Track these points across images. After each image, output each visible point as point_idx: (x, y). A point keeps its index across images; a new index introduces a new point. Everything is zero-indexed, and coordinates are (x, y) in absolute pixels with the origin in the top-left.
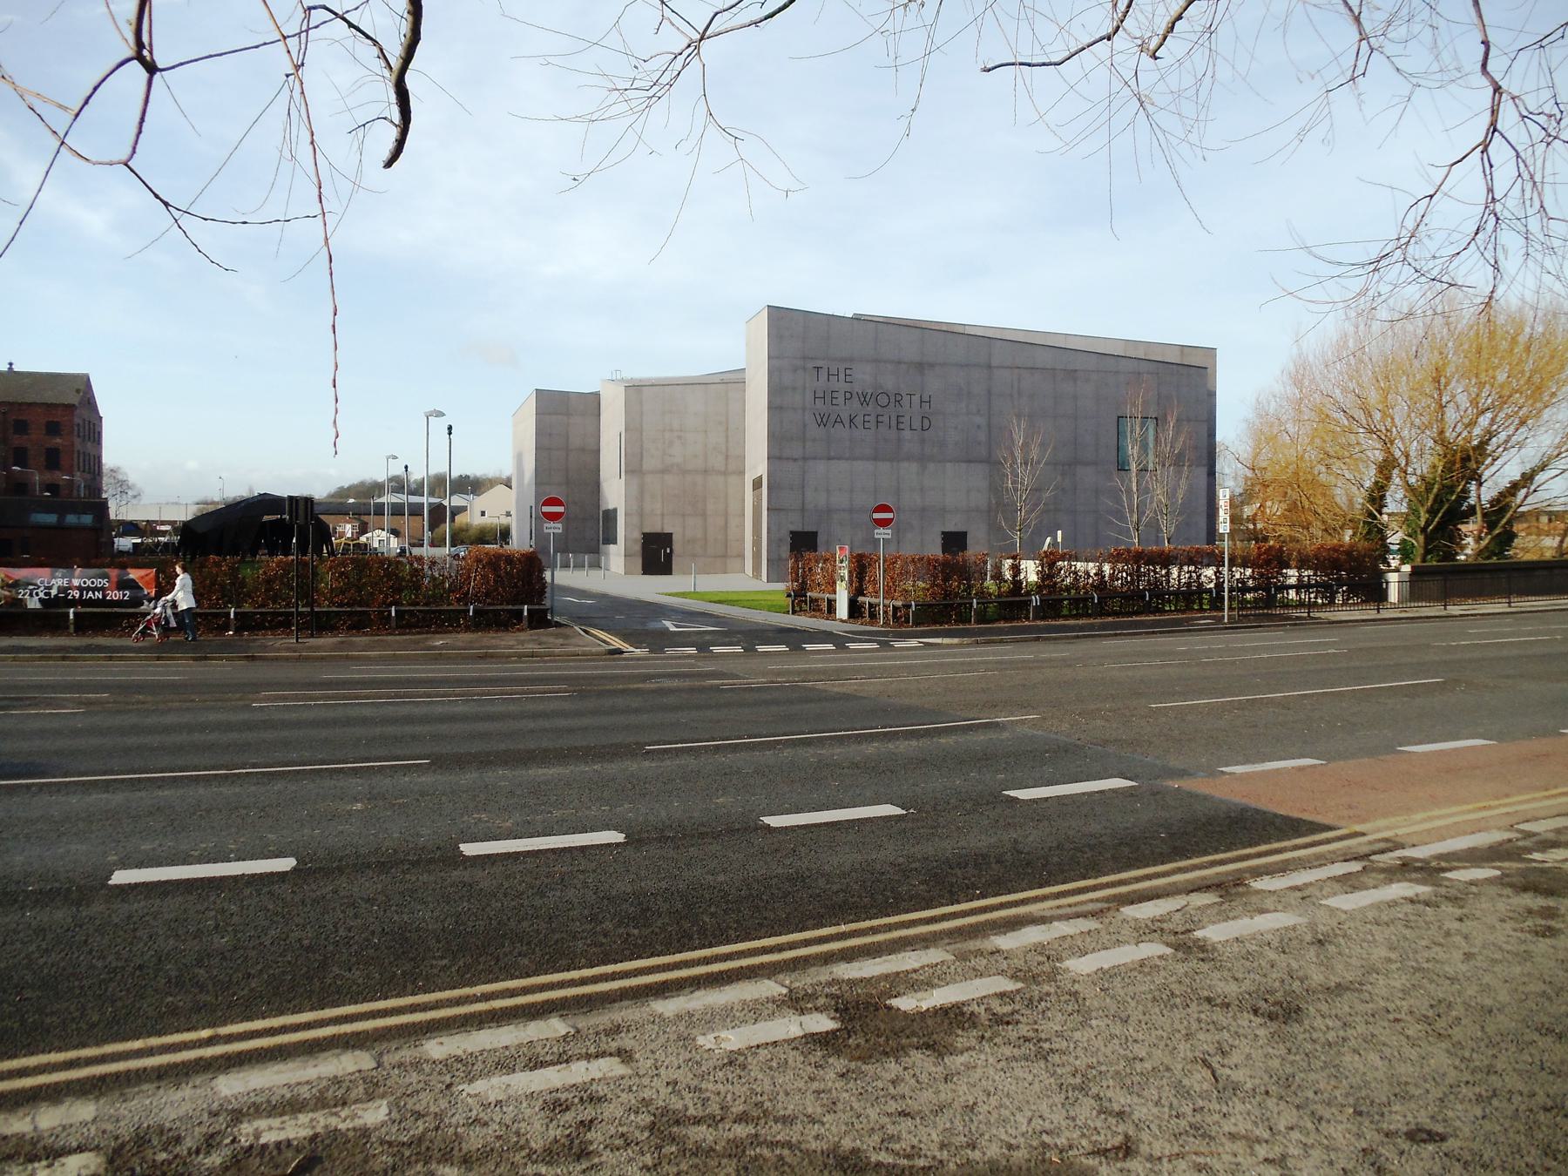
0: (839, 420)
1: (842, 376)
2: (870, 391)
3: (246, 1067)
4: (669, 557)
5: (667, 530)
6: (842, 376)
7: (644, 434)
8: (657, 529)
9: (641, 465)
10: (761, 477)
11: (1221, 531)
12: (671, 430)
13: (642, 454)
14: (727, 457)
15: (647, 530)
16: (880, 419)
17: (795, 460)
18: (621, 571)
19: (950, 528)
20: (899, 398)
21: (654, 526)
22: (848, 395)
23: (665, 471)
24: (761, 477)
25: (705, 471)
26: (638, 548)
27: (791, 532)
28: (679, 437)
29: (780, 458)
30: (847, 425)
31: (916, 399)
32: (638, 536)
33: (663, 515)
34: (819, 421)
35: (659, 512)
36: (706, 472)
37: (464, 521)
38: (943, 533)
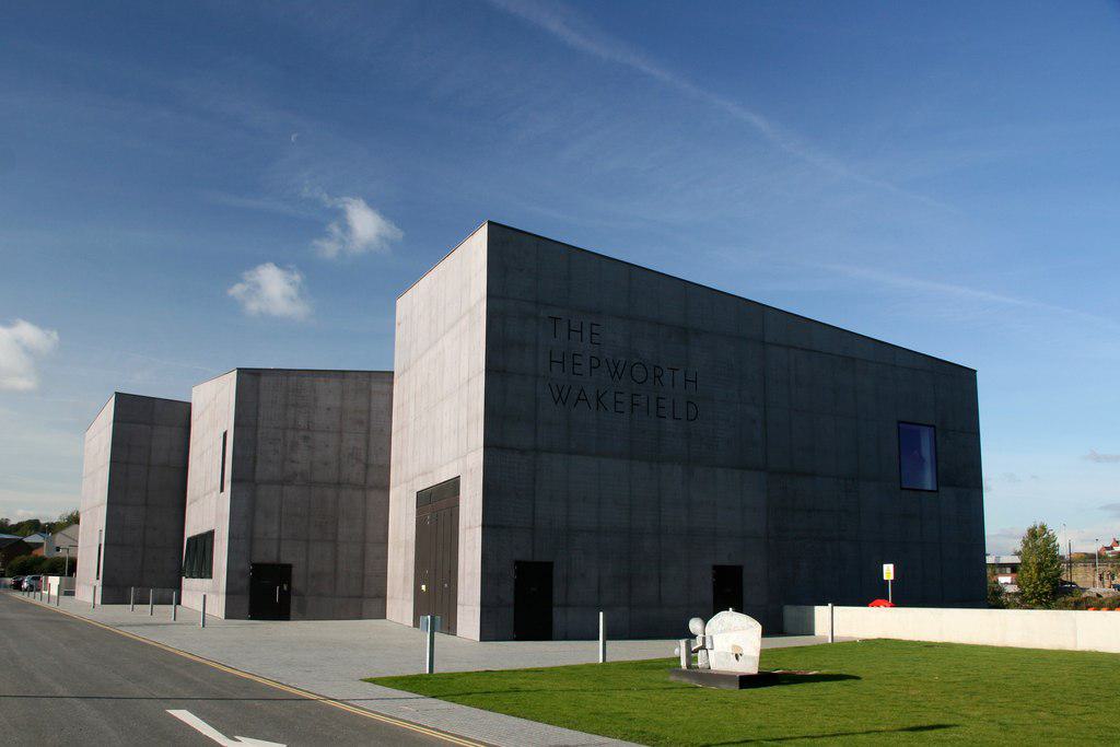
0: (582, 397)
1: (586, 334)
2: (623, 359)
3: (350, 223)
4: (286, 596)
5: (285, 560)
6: (586, 334)
7: (260, 432)
8: (271, 558)
9: (254, 470)
10: (453, 486)
11: (885, 578)
12: (296, 428)
13: (255, 457)
14: (367, 466)
15: (259, 558)
16: (636, 399)
17: (523, 452)
18: (476, 635)
19: (724, 561)
20: (658, 372)
21: (267, 554)
22: (595, 363)
23: (285, 481)
24: (453, 486)
25: (339, 483)
26: (244, 583)
27: (517, 563)
28: (306, 438)
29: (502, 448)
30: (593, 406)
31: (679, 375)
32: (245, 566)
33: (280, 539)
34: (557, 395)
35: (275, 536)
36: (339, 484)
37: (40, 555)
38: (715, 567)
